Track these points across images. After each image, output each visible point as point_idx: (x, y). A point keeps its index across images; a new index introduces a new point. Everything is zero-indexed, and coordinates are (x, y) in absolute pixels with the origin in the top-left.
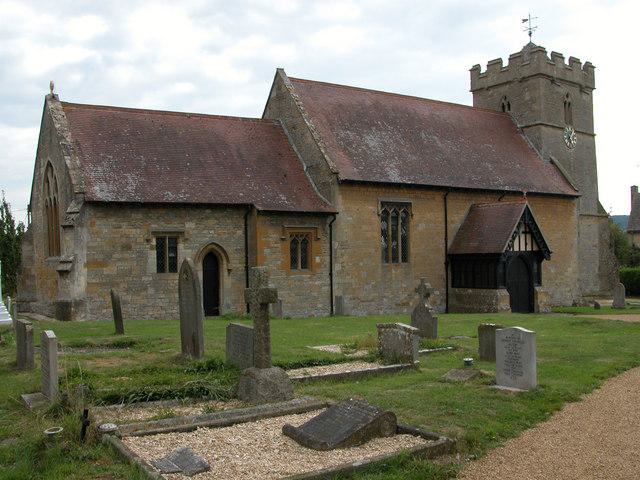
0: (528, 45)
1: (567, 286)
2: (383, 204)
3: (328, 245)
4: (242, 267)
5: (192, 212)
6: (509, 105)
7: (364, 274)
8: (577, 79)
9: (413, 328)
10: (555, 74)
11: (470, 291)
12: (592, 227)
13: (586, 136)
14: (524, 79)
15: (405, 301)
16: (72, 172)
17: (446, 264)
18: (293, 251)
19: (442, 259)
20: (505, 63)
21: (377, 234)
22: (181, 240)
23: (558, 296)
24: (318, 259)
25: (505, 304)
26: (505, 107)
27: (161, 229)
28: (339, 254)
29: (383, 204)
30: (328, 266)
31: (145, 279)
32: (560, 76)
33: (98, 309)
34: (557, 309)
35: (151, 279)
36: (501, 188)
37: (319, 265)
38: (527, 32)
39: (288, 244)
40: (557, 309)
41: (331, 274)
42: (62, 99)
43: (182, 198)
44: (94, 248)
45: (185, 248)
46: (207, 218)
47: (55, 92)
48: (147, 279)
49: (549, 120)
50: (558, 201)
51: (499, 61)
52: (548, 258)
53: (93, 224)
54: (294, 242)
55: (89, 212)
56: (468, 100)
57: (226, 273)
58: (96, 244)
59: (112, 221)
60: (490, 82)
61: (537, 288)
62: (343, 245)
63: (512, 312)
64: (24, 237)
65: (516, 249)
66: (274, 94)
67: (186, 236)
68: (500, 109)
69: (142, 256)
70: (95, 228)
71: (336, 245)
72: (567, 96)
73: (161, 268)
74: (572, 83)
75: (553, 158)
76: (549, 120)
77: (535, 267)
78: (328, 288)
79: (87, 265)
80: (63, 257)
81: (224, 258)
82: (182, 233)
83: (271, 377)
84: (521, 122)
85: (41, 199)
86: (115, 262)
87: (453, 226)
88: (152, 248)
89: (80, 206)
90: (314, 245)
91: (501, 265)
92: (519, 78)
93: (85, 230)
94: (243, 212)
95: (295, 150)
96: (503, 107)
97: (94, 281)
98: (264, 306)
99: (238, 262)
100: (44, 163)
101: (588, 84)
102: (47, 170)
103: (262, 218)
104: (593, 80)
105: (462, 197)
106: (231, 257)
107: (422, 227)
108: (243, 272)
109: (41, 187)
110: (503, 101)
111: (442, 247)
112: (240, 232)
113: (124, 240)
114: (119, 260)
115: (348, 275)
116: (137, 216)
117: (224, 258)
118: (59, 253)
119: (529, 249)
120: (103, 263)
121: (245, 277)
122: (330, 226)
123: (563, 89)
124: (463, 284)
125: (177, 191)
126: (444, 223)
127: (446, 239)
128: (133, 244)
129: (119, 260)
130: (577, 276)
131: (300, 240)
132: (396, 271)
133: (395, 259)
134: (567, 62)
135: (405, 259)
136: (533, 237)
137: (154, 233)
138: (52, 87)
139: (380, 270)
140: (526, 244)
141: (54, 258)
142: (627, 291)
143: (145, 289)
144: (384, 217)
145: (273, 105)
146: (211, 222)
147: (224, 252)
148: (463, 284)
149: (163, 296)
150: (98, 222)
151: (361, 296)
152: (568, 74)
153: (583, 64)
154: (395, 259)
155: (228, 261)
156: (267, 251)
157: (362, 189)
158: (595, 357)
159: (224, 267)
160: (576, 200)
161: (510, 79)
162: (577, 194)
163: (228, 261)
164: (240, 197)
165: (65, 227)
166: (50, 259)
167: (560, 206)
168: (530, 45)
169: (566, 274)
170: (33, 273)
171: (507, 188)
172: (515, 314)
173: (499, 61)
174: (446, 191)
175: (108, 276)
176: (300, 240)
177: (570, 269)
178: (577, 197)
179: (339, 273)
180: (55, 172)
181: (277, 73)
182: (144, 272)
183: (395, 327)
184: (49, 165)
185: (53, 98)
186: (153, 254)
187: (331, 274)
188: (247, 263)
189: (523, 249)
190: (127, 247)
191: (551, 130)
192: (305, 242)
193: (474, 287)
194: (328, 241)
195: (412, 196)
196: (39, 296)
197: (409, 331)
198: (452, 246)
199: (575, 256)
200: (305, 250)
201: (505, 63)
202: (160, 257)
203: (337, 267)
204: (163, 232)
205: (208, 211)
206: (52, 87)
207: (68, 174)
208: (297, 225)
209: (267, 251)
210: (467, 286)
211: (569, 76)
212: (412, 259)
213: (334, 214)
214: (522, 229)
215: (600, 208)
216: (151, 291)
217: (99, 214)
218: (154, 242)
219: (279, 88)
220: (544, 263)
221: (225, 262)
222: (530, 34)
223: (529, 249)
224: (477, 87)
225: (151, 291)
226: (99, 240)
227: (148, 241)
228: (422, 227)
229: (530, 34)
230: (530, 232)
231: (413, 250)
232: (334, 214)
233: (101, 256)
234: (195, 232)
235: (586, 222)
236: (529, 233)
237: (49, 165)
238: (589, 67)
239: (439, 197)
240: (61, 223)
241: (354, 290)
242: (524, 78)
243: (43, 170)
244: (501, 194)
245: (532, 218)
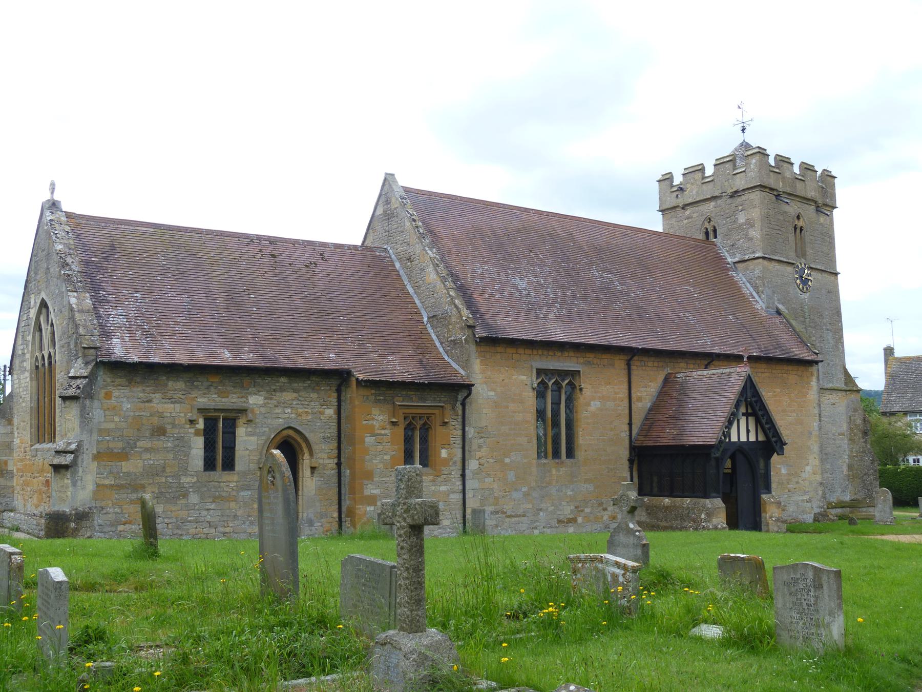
0: (742, 145)
1: (805, 493)
2: (539, 372)
3: (460, 433)
4: (332, 463)
5: (259, 381)
6: (715, 231)
7: (511, 476)
8: (811, 194)
9: (631, 563)
10: (780, 186)
11: (667, 501)
12: (839, 405)
13: (826, 275)
14: (735, 194)
15: (571, 516)
16: (78, 316)
17: (631, 461)
18: (408, 440)
19: (625, 453)
20: (709, 171)
21: (531, 417)
22: (241, 421)
23: (791, 509)
24: (444, 454)
25: (721, 519)
26: (710, 233)
27: (212, 405)
28: (474, 447)
29: (539, 372)
30: (459, 464)
31: (185, 480)
32: (788, 190)
33: (112, 525)
34: (794, 527)
35: (195, 479)
36: (708, 350)
37: (446, 462)
38: (739, 127)
39: (400, 431)
40: (794, 527)
41: (463, 476)
42: (66, 207)
43: (245, 359)
44: (108, 432)
45: (249, 434)
46: (282, 390)
47: (56, 197)
48: (188, 479)
49: (774, 252)
50: (790, 368)
51: (701, 169)
52: (781, 452)
53: (108, 396)
54: (410, 428)
55: (103, 377)
56: (655, 223)
57: (308, 472)
58: (112, 426)
59: (139, 392)
60: (692, 195)
61: (764, 497)
62: (481, 432)
63: (730, 529)
64: (730, 458)
65: (734, 438)
66: (380, 211)
67: (250, 416)
68: (701, 237)
69: (182, 445)
70: (113, 401)
71: (471, 432)
72: (798, 218)
73: (209, 465)
74: (806, 200)
75: (780, 307)
76: (774, 252)
77: (762, 464)
78: (459, 497)
79: (97, 457)
80: (60, 444)
81: (304, 445)
82: (243, 411)
83: (429, 647)
84: (733, 255)
85: (28, 356)
86: (141, 452)
87: (640, 405)
88: (197, 433)
89: (90, 367)
90: (438, 434)
91: (713, 463)
92: (729, 191)
93: (96, 403)
94: (335, 382)
95: (411, 291)
96: (707, 233)
97: (107, 482)
98: (416, 529)
99: (325, 456)
100: (34, 302)
101: (828, 201)
102: (39, 313)
103: (364, 392)
104: (833, 196)
105: (651, 363)
106: (315, 447)
107: (595, 405)
108: (334, 472)
109: (30, 338)
110: (707, 225)
111: (625, 435)
112: (330, 412)
113: (156, 421)
114: (147, 450)
115: (489, 475)
116: (176, 385)
117: (304, 445)
118: (52, 439)
119: (752, 438)
120: (123, 456)
121: (335, 480)
122: (463, 405)
123: (793, 208)
124: (655, 490)
125: (235, 345)
126: (627, 400)
127: (630, 424)
128: (168, 427)
129: (147, 450)
130: (818, 478)
131: (419, 424)
132: (558, 471)
133: (556, 454)
134: (796, 170)
135: (570, 454)
136: (758, 422)
137: (200, 410)
138: (52, 190)
139: (534, 469)
140: (748, 431)
141: (46, 446)
142: (894, 498)
143: (185, 496)
144: (541, 393)
145: (378, 226)
146: (288, 396)
147: (306, 440)
148: (655, 490)
149: (213, 506)
150: (116, 393)
151: (508, 508)
152: (799, 185)
153: (819, 173)
154: (556, 454)
155: (311, 454)
156: (369, 440)
157: (509, 350)
158: (112, 486)
159: (306, 462)
160: (815, 368)
161: (716, 194)
162: (815, 358)
163: (311, 454)
164: (331, 361)
165: (64, 398)
166: (37, 446)
167: (792, 375)
168: (745, 145)
169: (803, 475)
170: (10, 468)
171: (716, 350)
172: (732, 532)
173: (701, 169)
174: (630, 354)
175: (128, 474)
176: (419, 424)
177: (808, 468)
178: (817, 362)
179: (476, 473)
180: (52, 316)
181: (385, 180)
182: (185, 470)
183: (601, 560)
184: (44, 305)
185: (53, 205)
186: (198, 443)
187: (463, 476)
188: (339, 457)
189: (743, 438)
190: (160, 431)
191: (778, 266)
192: (426, 429)
193: (671, 495)
194: (459, 427)
195: (581, 360)
196: (18, 503)
197: (625, 568)
198: (638, 434)
199: (815, 448)
200: (424, 441)
201: (709, 171)
202: (209, 446)
203: (472, 465)
204: (216, 410)
205: (283, 380)
206: (52, 190)
207: (72, 318)
208: (415, 402)
209: (369, 440)
210: (661, 494)
211: (800, 189)
212: (580, 454)
213: (469, 387)
214: (743, 410)
215: (849, 379)
216: (194, 498)
217: (118, 381)
218: (201, 425)
219: (388, 202)
220: (775, 458)
221: (307, 455)
222: (743, 130)
223: (754, 439)
224: (665, 207)
225: (194, 498)
226: (116, 419)
227: (192, 422)
228: (595, 405)
229: (743, 130)
230: (754, 414)
231: (583, 439)
232: (469, 387)
233: (120, 445)
234: (263, 410)
235: (828, 399)
236: (751, 415)
237: (44, 305)
238: (828, 178)
239: (620, 363)
240: (57, 392)
241: (496, 499)
242: (736, 192)
243: (33, 313)
244: (709, 359)
245: (756, 394)
